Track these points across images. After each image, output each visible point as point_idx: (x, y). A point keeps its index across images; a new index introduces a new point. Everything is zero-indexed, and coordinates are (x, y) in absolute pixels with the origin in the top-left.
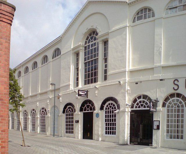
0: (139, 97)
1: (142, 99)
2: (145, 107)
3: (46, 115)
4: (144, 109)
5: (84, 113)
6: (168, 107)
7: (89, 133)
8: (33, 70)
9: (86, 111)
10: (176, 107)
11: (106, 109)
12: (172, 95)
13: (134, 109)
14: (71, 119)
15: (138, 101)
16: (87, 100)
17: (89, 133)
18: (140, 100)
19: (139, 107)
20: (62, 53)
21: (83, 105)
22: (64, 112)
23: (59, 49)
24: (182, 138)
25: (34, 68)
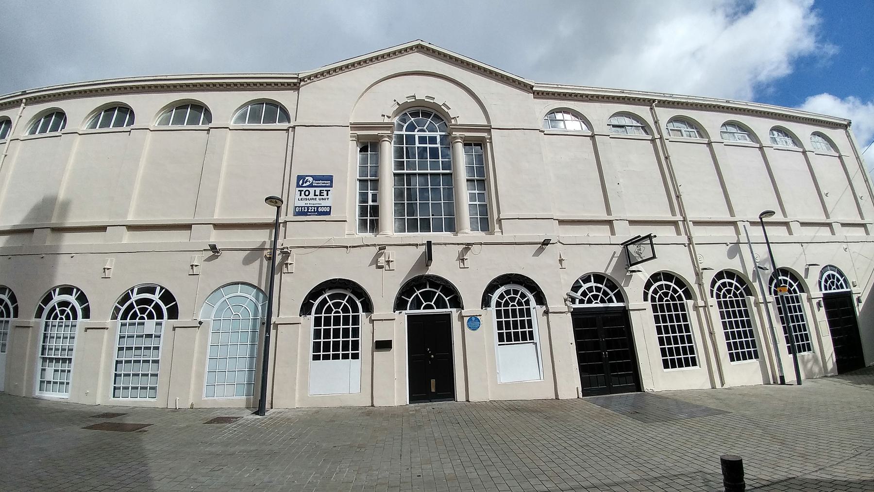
0: (586, 279)
1: (592, 284)
2: (602, 301)
3: (16, 316)
4: (601, 305)
5: (410, 318)
6: (653, 299)
7: (433, 381)
8: (33, 136)
9: (422, 311)
10: (669, 301)
11: (498, 304)
12: (599, 278)
13: (577, 305)
14: (803, 345)
15: (585, 286)
16: (422, 277)
17: (433, 381)
18: (588, 285)
19: (589, 301)
20: (67, 129)
21: (407, 289)
22: (305, 309)
23: (65, 114)
24: (316, 358)
25: (43, 130)
